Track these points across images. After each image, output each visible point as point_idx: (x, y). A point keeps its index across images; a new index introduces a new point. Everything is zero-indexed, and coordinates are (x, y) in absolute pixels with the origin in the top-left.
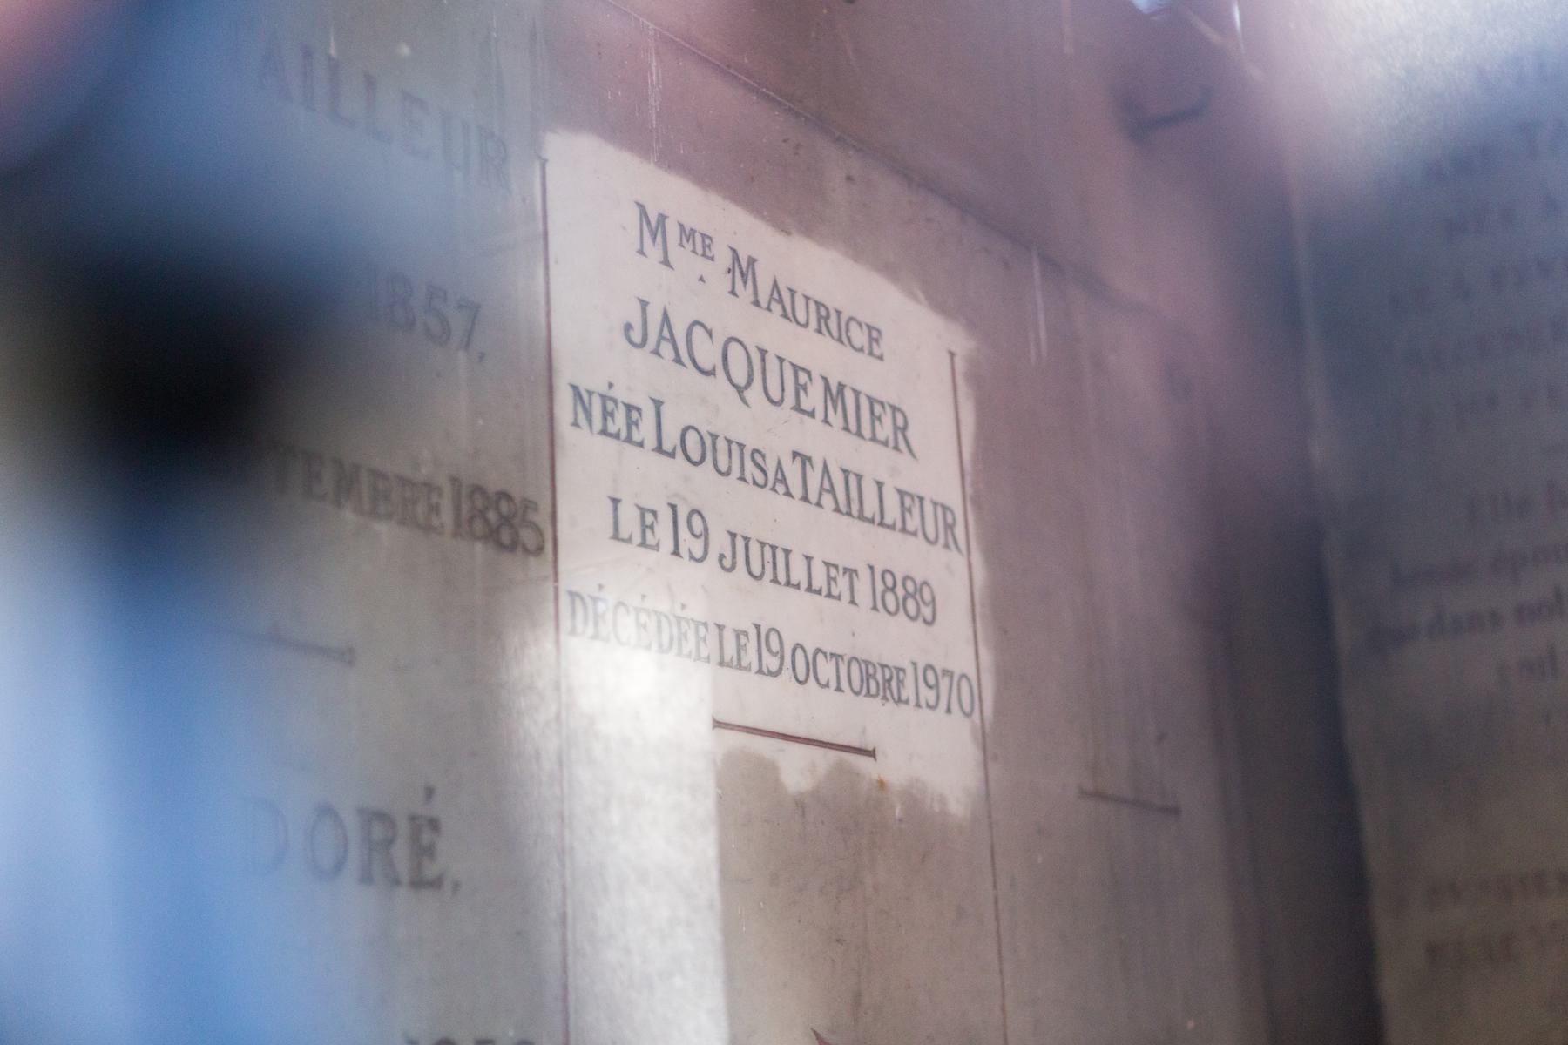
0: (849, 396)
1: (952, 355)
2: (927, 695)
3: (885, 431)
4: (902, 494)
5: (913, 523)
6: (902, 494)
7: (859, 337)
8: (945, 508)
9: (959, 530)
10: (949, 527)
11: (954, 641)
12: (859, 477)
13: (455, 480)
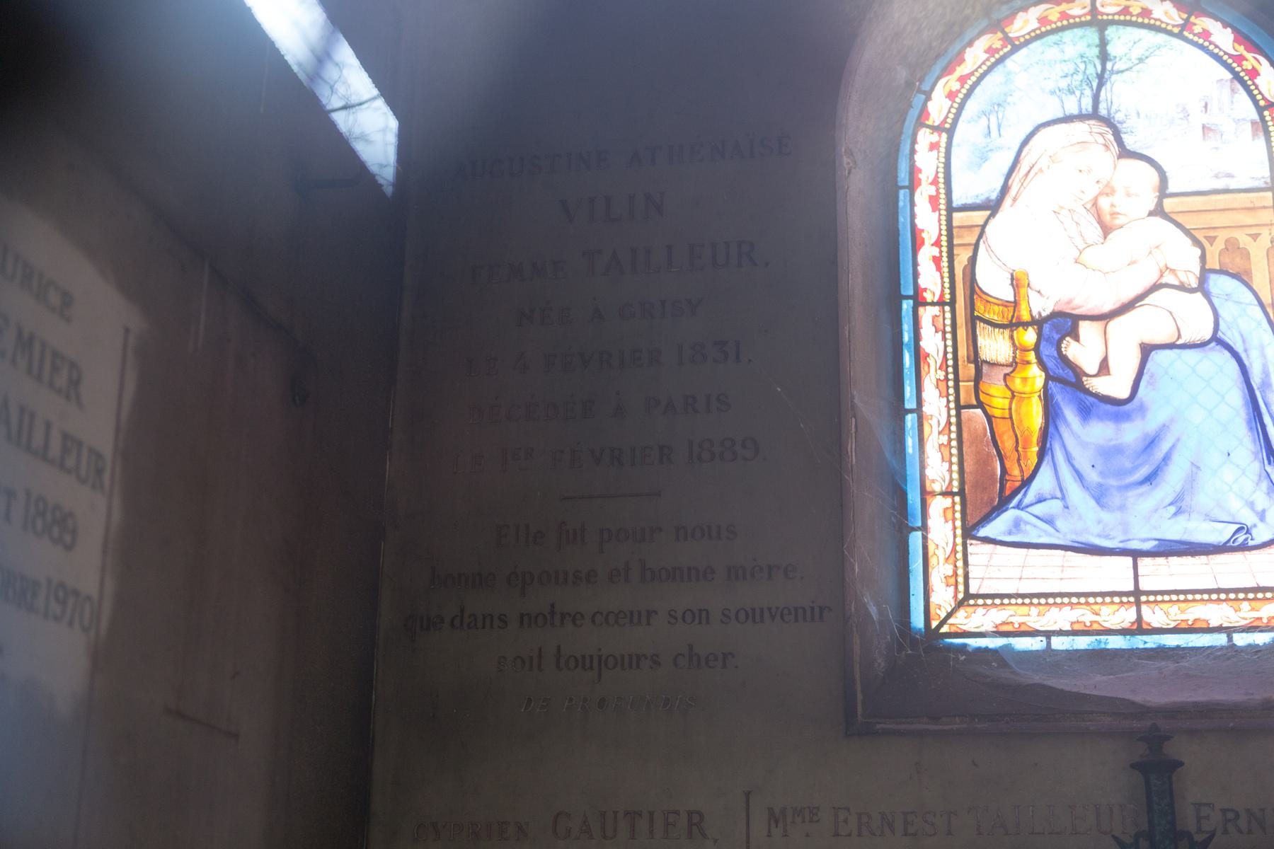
0: (37, 347)
1: (127, 331)
2: (55, 608)
3: (61, 381)
4: (66, 437)
5: (70, 462)
6: (66, 437)
7: (54, 298)
8: (99, 456)
9: (107, 476)
10: (99, 472)
11: (86, 568)
12: (32, 416)
13: (49, 581)
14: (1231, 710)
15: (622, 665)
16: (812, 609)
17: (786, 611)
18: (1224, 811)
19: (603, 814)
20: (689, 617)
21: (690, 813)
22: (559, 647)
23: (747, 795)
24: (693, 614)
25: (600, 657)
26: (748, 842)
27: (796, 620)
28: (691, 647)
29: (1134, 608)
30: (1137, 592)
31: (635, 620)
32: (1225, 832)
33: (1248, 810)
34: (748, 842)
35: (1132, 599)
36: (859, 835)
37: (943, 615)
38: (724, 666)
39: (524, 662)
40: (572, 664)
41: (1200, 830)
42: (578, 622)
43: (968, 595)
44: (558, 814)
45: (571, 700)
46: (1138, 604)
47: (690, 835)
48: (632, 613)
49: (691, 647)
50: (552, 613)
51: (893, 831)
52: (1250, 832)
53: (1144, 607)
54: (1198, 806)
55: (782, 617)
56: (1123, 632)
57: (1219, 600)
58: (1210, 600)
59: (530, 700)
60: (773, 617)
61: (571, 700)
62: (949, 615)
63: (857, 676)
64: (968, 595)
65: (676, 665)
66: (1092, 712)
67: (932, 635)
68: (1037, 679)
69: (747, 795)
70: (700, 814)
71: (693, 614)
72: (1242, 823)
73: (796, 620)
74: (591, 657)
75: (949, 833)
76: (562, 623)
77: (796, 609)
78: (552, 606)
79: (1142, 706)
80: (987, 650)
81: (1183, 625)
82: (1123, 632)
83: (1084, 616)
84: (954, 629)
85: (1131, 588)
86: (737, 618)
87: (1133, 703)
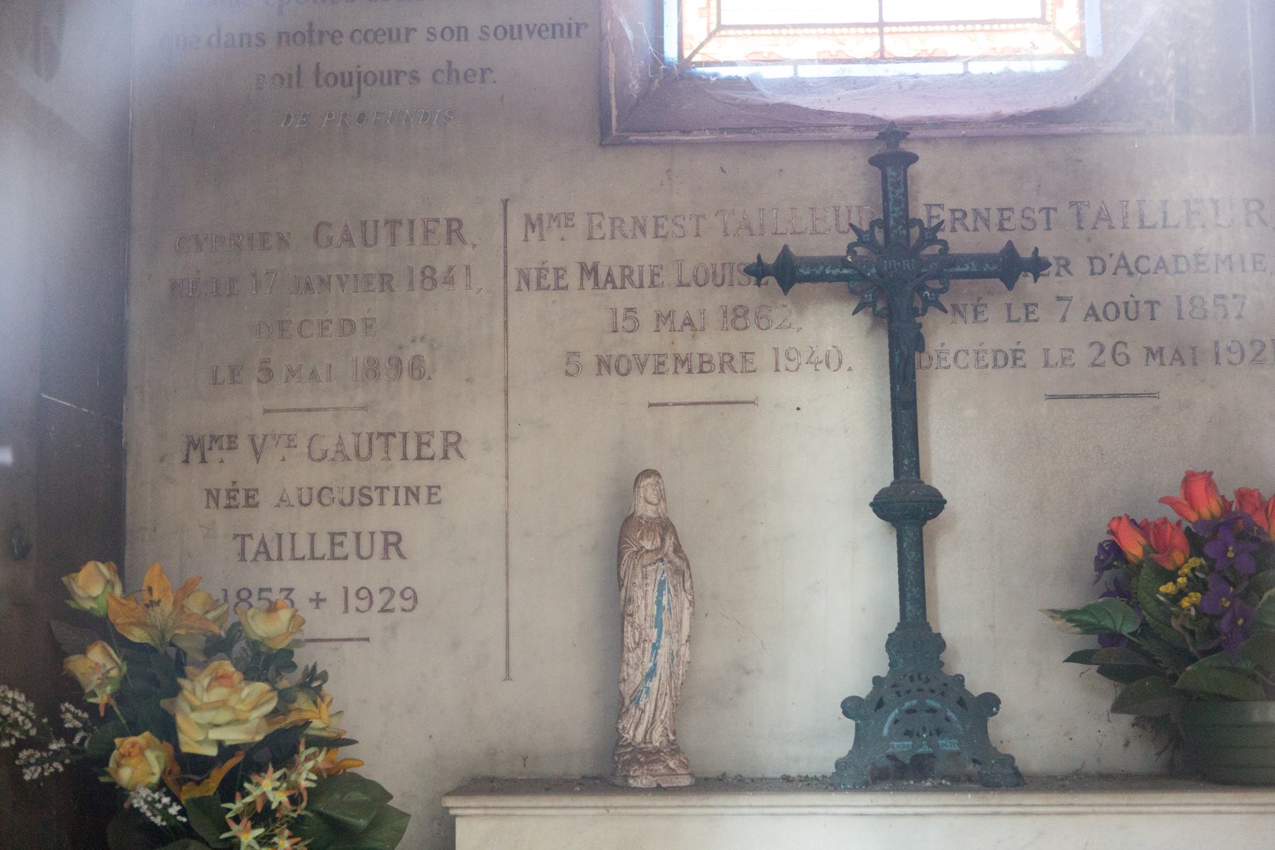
14: (965, 122)
15: (382, 81)
16: (569, 25)
17: (543, 28)
18: (953, 211)
19: (364, 224)
20: (447, 34)
21: (449, 221)
22: (318, 64)
23: (505, 203)
24: (452, 31)
25: (359, 73)
26: (505, 247)
27: (554, 37)
28: (450, 63)
29: (878, 38)
30: (881, 24)
31: (394, 38)
32: (954, 230)
33: (975, 210)
34: (505, 247)
35: (876, 30)
36: (613, 238)
37: (696, 46)
38: (483, 81)
39: (282, 78)
40: (331, 81)
41: (930, 218)
42: (337, 40)
43: (720, 27)
44: (319, 225)
45: (330, 115)
46: (881, 34)
47: (449, 241)
48: (390, 31)
49: (450, 63)
50: (311, 31)
51: (644, 233)
52: (976, 229)
53: (886, 38)
54: (929, 206)
55: (540, 34)
56: (868, 61)
57: (958, 31)
58: (950, 32)
59: (289, 116)
60: (531, 33)
61: (330, 115)
62: (702, 45)
63: (613, 92)
64: (720, 27)
65: (435, 80)
66: (834, 126)
67: (684, 63)
68: (783, 99)
69: (505, 203)
70: (459, 221)
71: (452, 31)
72: (969, 221)
73: (554, 37)
74: (350, 74)
75: (698, 235)
76: (321, 41)
77: (553, 25)
78: (311, 24)
79: (881, 119)
80: (738, 79)
81: (924, 55)
82: (868, 61)
83: (830, 46)
84: (705, 59)
85: (877, 20)
86: (495, 34)
87: (873, 117)
